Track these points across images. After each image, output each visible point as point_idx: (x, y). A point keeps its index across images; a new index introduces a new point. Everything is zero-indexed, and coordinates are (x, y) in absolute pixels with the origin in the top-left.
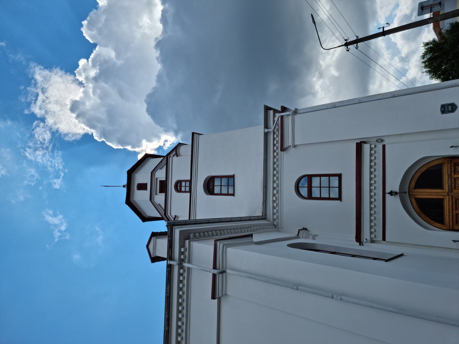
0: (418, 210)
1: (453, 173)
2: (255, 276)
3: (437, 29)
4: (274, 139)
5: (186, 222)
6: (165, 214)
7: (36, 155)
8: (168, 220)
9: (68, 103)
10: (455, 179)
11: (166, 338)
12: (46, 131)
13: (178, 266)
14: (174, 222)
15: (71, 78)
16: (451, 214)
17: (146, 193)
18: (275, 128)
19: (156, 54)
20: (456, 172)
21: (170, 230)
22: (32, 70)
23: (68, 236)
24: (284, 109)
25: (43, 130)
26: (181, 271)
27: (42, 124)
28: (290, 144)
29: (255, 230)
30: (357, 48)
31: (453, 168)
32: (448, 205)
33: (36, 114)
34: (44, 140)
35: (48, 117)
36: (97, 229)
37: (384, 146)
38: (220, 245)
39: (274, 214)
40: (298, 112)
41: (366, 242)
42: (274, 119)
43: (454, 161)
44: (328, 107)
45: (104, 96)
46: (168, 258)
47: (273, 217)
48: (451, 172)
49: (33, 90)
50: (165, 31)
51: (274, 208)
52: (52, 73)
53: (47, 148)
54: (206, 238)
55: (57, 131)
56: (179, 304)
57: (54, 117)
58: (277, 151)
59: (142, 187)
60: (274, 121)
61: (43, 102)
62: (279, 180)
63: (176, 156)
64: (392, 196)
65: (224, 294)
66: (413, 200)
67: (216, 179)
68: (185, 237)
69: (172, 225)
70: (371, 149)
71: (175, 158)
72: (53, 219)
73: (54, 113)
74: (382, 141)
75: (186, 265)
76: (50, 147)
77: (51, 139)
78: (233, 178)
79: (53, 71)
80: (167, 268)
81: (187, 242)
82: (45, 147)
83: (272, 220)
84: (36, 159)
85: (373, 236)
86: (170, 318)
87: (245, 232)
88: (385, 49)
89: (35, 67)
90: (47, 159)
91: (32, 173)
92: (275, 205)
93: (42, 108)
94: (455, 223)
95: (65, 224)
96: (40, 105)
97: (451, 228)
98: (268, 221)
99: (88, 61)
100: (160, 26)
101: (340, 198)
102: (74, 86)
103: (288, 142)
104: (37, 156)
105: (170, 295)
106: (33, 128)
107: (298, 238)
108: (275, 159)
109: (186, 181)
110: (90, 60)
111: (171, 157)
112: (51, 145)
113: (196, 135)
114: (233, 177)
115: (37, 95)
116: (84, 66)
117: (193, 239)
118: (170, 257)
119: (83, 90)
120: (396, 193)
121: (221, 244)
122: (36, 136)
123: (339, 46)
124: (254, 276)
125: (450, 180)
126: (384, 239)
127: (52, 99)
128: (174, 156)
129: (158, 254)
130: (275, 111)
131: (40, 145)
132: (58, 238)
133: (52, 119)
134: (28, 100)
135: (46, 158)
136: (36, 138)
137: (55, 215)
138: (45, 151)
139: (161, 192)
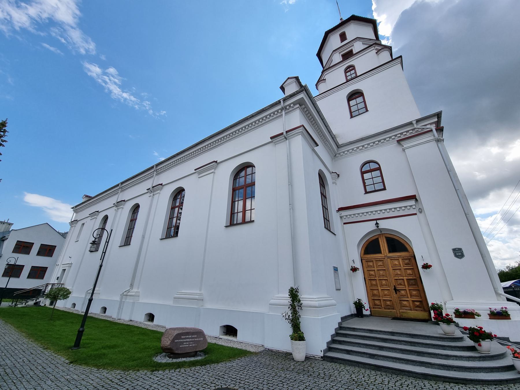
0: (370, 240)
1: (402, 258)
2: (289, 159)
4: (407, 132)
18: (418, 128)
20: (404, 260)
26: (280, 111)
28: (405, 146)
31: (407, 258)
39: (344, 152)
40: (439, 143)
43: (412, 258)
47: (341, 152)
48: (403, 257)
51: (348, 151)
54: (306, 117)
58: (396, 138)
62: (382, 144)
63: (376, 51)
64: (375, 224)
65: (275, 143)
66: (377, 237)
67: (361, 98)
71: (375, 51)
75: (283, 113)
81: (298, 106)
83: (339, 152)
85: (345, 217)
97: (362, 259)
98: (337, 150)
101: (366, 192)
108: (394, 136)
109: (355, 73)
111: (374, 48)
114: (367, 111)
117: (301, 108)
120: (378, 227)
121: (302, 130)
124: (289, 158)
125: (397, 257)
126: (345, 224)
139: (343, 56)
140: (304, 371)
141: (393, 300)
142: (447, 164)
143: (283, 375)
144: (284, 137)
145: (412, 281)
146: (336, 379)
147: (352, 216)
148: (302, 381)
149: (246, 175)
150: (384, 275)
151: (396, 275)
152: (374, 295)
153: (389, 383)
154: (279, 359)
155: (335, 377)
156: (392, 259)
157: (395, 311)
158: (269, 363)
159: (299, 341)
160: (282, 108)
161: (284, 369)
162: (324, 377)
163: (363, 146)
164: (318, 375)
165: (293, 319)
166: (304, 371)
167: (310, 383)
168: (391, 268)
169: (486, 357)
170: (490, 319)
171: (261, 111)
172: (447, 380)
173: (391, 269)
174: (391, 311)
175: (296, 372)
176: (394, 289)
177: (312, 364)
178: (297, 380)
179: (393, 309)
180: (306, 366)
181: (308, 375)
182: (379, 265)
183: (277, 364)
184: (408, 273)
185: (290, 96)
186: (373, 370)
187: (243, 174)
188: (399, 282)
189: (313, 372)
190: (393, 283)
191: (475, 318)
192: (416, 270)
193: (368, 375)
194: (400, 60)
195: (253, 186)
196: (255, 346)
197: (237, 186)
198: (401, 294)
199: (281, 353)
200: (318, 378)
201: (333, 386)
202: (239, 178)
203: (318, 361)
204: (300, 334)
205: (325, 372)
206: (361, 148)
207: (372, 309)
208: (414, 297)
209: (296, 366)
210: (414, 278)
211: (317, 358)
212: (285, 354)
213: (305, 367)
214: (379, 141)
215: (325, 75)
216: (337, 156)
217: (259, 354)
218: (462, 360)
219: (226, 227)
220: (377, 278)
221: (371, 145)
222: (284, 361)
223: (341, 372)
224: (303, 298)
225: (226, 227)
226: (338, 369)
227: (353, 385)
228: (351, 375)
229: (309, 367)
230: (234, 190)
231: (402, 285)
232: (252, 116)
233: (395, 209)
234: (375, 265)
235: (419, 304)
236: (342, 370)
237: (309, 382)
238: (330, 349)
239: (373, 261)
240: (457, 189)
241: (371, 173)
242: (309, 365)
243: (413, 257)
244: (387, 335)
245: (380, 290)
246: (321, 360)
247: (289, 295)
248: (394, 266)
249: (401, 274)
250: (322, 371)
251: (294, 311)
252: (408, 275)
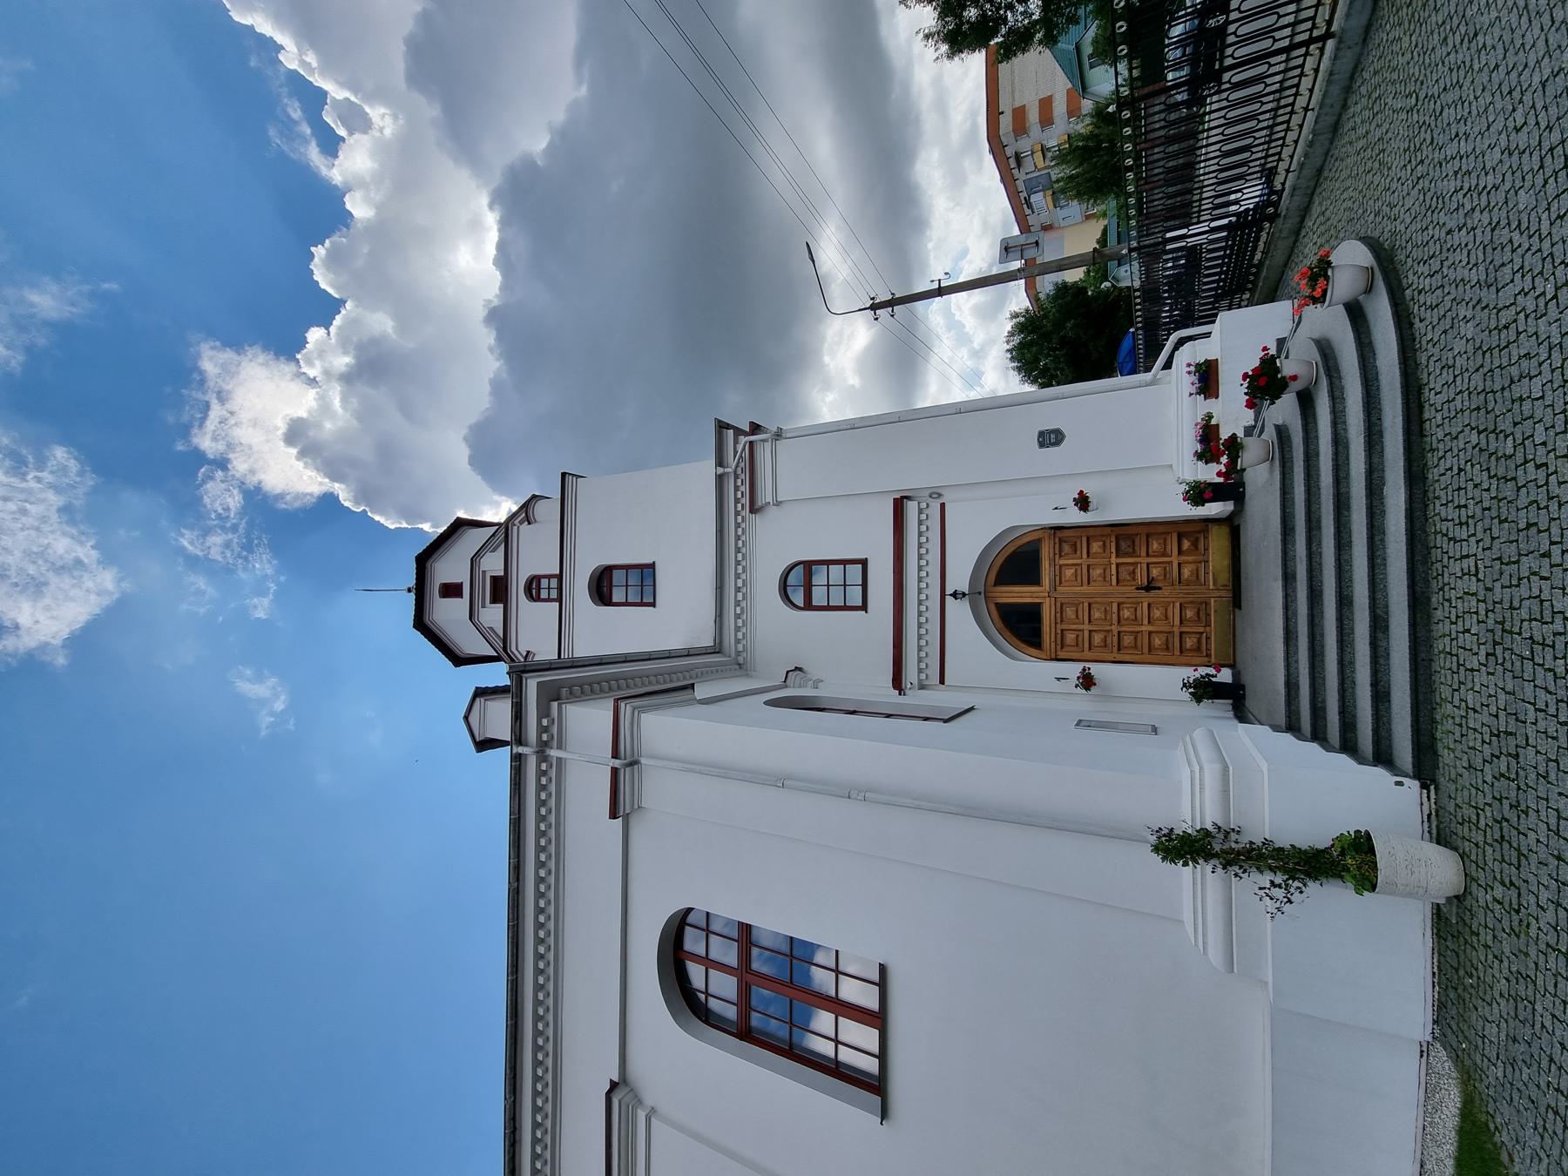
1: (1057, 556)
3: (1031, 289)
4: (736, 488)
5: (551, 663)
6: (505, 649)
7: (207, 544)
8: (512, 660)
9: (282, 427)
10: (1061, 566)
11: (512, 969)
12: (231, 488)
13: (535, 757)
14: (525, 666)
15: (289, 368)
16: (1053, 630)
17: (460, 606)
18: (737, 466)
19: (487, 337)
20: (1063, 554)
21: (516, 681)
22: (192, 349)
23: (292, 722)
24: (756, 428)
25: (223, 486)
27: (219, 474)
28: (769, 499)
29: (699, 674)
30: (892, 316)
31: (1057, 546)
32: (1048, 614)
33: (204, 451)
34: (228, 509)
35: (235, 458)
36: (367, 714)
37: (943, 506)
38: (626, 709)
39: (738, 641)
40: (784, 435)
41: (910, 689)
42: (735, 448)
43: (1059, 534)
44: (841, 428)
45: (366, 414)
46: (514, 742)
48: (1055, 554)
49: (200, 395)
50: (505, 287)
51: (737, 629)
52: (242, 356)
53: (234, 528)
55: (258, 489)
56: (541, 834)
57: (249, 458)
58: (743, 513)
59: (451, 590)
60: (735, 452)
61: (220, 423)
63: (526, 523)
64: (956, 599)
65: (636, 807)
66: (993, 607)
67: (616, 573)
68: (550, 695)
69: (520, 671)
70: (920, 511)
72: (255, 687)
73: (250, 447)
74: (940, 495)
75: (554, 753)
76: (241, 526)
77: (243, 507)
78: (651, 570)
79: (246, 351)
80: (511, 762)
81: (555, 704)
82: (228, 525)
83: (733, 655)
84: (209, 553)
86: (521, 864)
87: (678, 680)
88: (944, 329)
89: (199, 343)
90: (236, 553)
91: (200, 587)
92: (740, 622)
93: (218, 438)
94: (1059, 647)
95: (283, 697)
96: (214, 431)
98: (725, 656)
99: (329, 334)
100: (497, 277)
101: (864, 607)
102: (296, 387)
103: (765, 495)
104: (209, 548)
105: (519, 817)
106: (197, 482)
107: (786, 687)
109: (549, 577)
110: (333, 329)
112: (244, 521)
113: (571, 477)
115: (207, 406)
116: (318, 342)
118: (519, 738)
119: (317, 393)
120: (964, 595)
121: (628, 706)
122: (206, 500)
123: (860, 310)
125: (1052, 569)
126: (942, 681)
127: (244, 416)
128: (521, 522)
129: (492, 734)
130: (738, 432)
131: (216, 522)
132: (267, 727)
133: (245, 461)
134: (185, 418)
135: (233, 550)
136: (205, 506)
137: (259, 678)
138: (230, 536)
139: (494, 600)
140: (1502, 837)
141: (1182, 600)
142: (837, 428)
143: (1549, 916)
144: (627, 769)
145: (1123, 545)
146: (1505, 710)
147: (923, 643)
148: (1555, 829)
149: (708, 962)
150: (1105, 609)
151: (1104, 578)
152: (1167, 647)
153: (1467, 556)
154: (1475, 962)
155: (1497, 716)
156: (1058, 581)
157: (1212, 600)
158: (1503, 1002)
159: (1378, 857)
160: (537, 752)
161: (1515, 924)
162: (1510, 755)
163: (738, 590)
164: (1509, 779)
165: (1285, 871)
166: (1502, 837)
167: (1553, 796)
168: (1085, 587)
169: (1327, 365)
170: (1217, 397)
171: (515, 830)
172: (1415, 428)
173: (1085, 589)
174: (1215, 611)
175: (1518, 869)
176: (1147, 591)
177: (1463, 819)
178: (1556, 853)
179: (1207, 604)
180: (1480, 838)
181: (1519, 817)
182: (1074, 617)
183: (1501, 961)
184: (1100, 550)
185: (516, 716)
186: (1429, 617)
187: (696, 973)
188: (1124, 575)
189: (1500, 800)
190: (1129, 590)
191: (1218, 425)
192: (1091, 532)
193: (1456, 623)
194: (571, 477)
195: (754, 938)
196: (1430, 1091)
197: (731, 1012)
198: (1162, 578)
199: (1442, 959)
200: (1521, 773)
201: (1536, 710)
202: (707, 993)
203: (1444, 801)
204: (1346, 846)
205: (1485, 761)
206: (740, 556)
207: (1213, 660)
208: (1169, 547)
209: (1490, 878)
210: (1113, 539)
211: (1433, 806)
212: (1445, 940)
213: (1485, 842)
214: (738, 550)
215: (517, 649)
216: (741, 662)
217: (1467, 1062)
218: (1343, 411)
219: (884, 1114)
220: (1115, 629)
221: (740, 571)
222: (1478, 935)
223: (1467, 707)
224: (1193, 819)
225: (884, 1114)
226: (1458, 720)
227: (1512, 650)
228: (1472, 670)
229: (1482, 824)
230: (744, 1032)
231: (1134, 570)
232: (516, 870)
233: (923, 545)
234: (1074, 627)
235: (1189, 541)
236: (1459, 708)
237: (1547, 800)
238: (1383, 757)
239: (1062, 630)
240: (897, 420)
241: (813, 588)
242: (1473, 827)
243: (1055, 533)
244: (1295, 591)
245: (1151, 628)
246: (1436, 794)
247: (1183, 865)
248: (1079, 577)
249: (1103, 567)
250: (1482, 771)
251: (1249, 858)
252: (1104, 552)
